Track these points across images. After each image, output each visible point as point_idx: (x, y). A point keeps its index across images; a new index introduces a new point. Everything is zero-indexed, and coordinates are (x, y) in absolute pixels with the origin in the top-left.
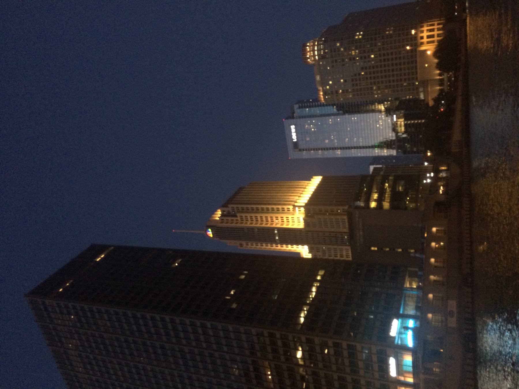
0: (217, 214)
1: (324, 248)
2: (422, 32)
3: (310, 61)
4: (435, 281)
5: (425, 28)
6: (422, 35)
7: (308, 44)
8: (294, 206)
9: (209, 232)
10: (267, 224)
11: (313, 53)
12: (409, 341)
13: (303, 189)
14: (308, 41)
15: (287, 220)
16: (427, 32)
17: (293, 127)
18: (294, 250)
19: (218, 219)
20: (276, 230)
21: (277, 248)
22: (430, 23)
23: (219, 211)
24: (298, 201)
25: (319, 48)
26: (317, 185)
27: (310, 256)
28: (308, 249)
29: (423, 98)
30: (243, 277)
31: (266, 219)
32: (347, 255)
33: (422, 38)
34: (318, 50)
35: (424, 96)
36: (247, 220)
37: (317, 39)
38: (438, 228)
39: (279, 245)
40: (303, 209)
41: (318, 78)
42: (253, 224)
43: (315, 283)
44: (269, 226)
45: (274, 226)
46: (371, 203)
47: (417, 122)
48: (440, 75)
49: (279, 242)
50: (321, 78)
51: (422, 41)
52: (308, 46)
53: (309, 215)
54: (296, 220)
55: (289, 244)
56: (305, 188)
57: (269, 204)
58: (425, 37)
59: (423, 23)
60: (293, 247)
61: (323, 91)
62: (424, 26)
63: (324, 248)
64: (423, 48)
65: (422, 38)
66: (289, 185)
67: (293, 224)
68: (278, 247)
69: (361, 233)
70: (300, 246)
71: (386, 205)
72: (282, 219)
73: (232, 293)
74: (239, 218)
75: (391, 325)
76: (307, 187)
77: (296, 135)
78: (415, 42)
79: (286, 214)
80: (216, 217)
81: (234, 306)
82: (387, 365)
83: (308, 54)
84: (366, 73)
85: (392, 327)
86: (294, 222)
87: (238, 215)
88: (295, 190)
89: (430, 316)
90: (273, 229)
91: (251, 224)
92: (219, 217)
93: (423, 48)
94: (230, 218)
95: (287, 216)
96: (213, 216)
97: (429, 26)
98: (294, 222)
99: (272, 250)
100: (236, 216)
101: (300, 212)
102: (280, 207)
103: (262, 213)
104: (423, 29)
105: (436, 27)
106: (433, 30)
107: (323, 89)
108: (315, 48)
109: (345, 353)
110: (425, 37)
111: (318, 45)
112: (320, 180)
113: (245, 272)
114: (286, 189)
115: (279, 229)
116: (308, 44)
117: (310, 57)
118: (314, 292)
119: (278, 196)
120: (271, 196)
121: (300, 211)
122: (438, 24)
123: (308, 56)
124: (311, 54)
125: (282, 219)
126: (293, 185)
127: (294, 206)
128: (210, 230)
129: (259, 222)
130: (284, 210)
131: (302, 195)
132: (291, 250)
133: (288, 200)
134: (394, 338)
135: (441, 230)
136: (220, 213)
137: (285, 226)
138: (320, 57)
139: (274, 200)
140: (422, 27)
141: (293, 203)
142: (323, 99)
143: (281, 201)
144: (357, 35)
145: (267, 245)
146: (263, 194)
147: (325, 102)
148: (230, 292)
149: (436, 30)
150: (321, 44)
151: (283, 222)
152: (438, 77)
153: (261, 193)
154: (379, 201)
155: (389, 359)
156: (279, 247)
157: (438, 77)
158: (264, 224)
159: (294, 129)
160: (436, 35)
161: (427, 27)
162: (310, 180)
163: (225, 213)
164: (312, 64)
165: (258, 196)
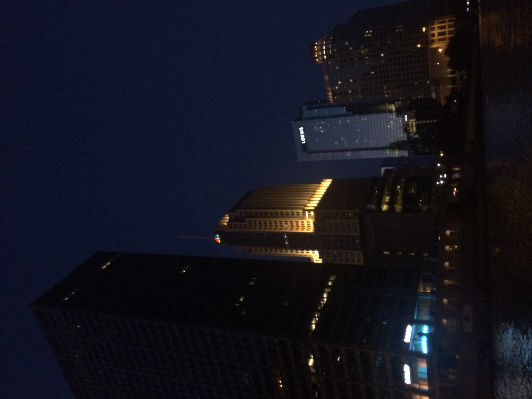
0: (225, 219)
1: (335, 253)
2: (433, 29)
4: (449, 285)
5: (436, 26)
6: (433, 32)
7: (316, 44)
8: (304, 211)
9: (217, 237)
11: (321, 53)
13: (312, 193)
16: (438, 30)
17: (301, 129)
19: (226, 224)
20: (285, 235)
21: (287, 253)
23: (227, 217)
24: (308, 205)
27: (320, 261)
33: (433, 35)
34: (326, 50)
40: (312, 213)
41: (327, 78)
44: (278, 230)
45: (283, 230)
48: (452, 73)
51: (433, 38)
52: (316, 45)
54: (306, 224)
55: (305, 250)
56: (315, 191)
58: (436, 35)
65: (433, 35)
70: (310, 252)
71: (398, 208)
72: (297, 223)
73: (241, 300)
74: (247, 223)
80: (224, 222)
84: (376, 73)
87: (246, 220)
89: (445, 321)
90: (283, 234)
91: (250, 228)
92: (227, 223)
93: (434, 46)
94: (238, 224)
95: (291, 220)
100: (244, 221)
102: (289, 211)
105: (447, 24)
106: (444, 27)
107: (332, 89)
112: (330, 183)
115: (289, 234)
116: (316, 44)
125: (291, 224)
128: (218, 236)
133: (298, 204)
134: (408, 344)
136: (228, 218)
137: (294, 231)
140: (433, 24)
141: (303, 207)
146: (271, 198)
149: (447, 27)
154: (391, 204)
157: (450, 76)
159: (303, 131)
160: (447, 33)
162: (320, 183)
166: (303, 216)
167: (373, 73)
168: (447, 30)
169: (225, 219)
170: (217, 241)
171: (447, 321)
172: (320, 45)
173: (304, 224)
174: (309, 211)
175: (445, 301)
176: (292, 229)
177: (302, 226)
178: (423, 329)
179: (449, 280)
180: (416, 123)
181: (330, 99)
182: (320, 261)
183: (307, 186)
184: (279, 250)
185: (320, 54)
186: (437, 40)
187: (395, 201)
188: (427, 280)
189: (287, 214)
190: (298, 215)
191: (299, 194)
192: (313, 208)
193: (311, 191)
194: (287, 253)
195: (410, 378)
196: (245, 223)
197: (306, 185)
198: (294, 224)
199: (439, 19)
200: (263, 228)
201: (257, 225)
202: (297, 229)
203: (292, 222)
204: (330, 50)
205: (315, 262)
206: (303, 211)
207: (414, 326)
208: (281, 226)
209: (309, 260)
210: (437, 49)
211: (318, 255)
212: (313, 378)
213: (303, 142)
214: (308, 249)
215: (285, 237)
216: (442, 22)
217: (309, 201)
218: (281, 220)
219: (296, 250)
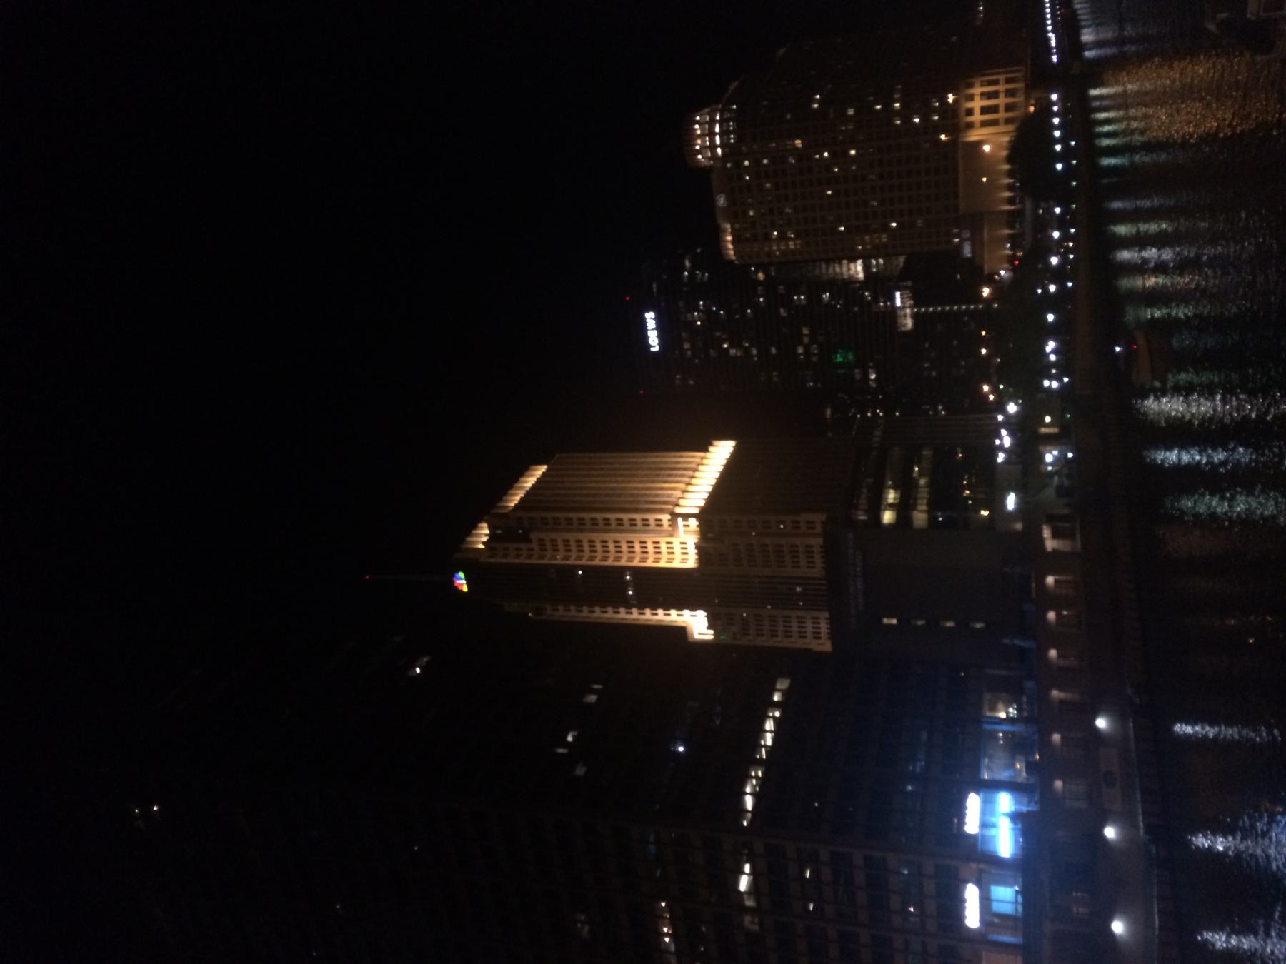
0: (480, 535)
1: (745, 615)
2: (971, 98)
3: (703, 160)
4: (1062, 702)
5: (977, 90)
6: (969, 105)
7: (698, 118)
8: (675, 516)
9: (460, 579)
10: (605, 559)
11: (710, 141)
12: (1005, 843)
13: (690, 473)
14: (698, 110)
15: (655, 548)
16: (981, 99)
17: (650, 318)
18: (671, 621)
19: (482, 546)
20: (628, 573)
21: (642, 617)
22: (990, 78)
23: (482, 528)
24: (682, 502)
25: (725, 128)
26: (724, 462)
27: (709, 635)
28: (706, 619)
29: (969, 255)
30: (592, 698)
31: (616, 547)
32: (800, 632)
33: (970, 112)
34: (721, 134)
35: (973, 251)
36: (554, 550)
37: (720, 106)
38: (1057, 577)
39: (635, 611)
40: (693, 523)
41: (721, 201)
42: (584, 559)
43: (770, 709)
44: (610, 562)
45: (623, 563)
46: (882, 512)
47: (941, 310)
48: (1010, 201)
49: (635, 602)
50: (731, 201)
51: (970, 119)
52: (698, 122)
53: (710, 535)
54: (677, 548)
55: (660, 608)
56: (696, 470)
57: (636, 510)
58: (977, 111)
59: (971, 77)
60: (682, 615)
61: (732, 233)
62: (976, 85)
63: (745, 615)
64: (973, 136)
65: (970, 112)
66: (654, 463)
67: (669, 559)
68: (606, 612)
69: (860, 585)
70: (686, 612)
71: (920, 517)
72: (631, 545)
73: (570, 739)
74: (534, 545)
75: (965, 808)
76: (701, 468)
77: (657, 337)
78: (954, 120)
79: (655, 533)
80: (477, 542)
81: (580, 771)
82: (959, 902)
83: (699, 141)
84: (836, 193)
85: (967, 812)
86: (673, 553)
87: (533, 536)
88: (670, 476)
89: (1058, 784)
90: (623, 570)
91: (543, 557)
92: (484, 543)
93: (973, 136)
95: (657, 540)
96: (469, 539)
97: (985, 83)
98: (673, 553)
99: (592, 620)
100: (530, 541)
101: (687, 529)
102: (638, 517)
103: (593, 531)
104: (971, 91)
105: (1001, 88)
106: (994, 95)
107: (732, 228)
108: (714, 128)
109: (860, 878)
110: (977, 111)
111: (721, 122)
112: (731, 450)
113: (596, 686)
114: (649, 472)
115: (637, 572)
116: (698, 118)
117: (703, 151)
118: (768, 732)
119: (631, 489)
120: (612, 489)
121: (688, 526)
122: (1008, 81)
123: (698, 147)
124: (706, 141)
125: (642, 547)
126: (666, 463)
127: (675, 516)
128: (461, 574)
129: (587, 553)
130: (648, 525)
131: (690, 488)
132: (638, 620)
133: (657, 499)
134: (974, 837)
135: (1065, 581)
136: (487, 532)
137: (650, 563)
138: (727, 150)
139: (622, 499)
140: (971, 86)
141: (670, 507)
142: (732, 253)
143: (639, 502)
144: (817, 99)
145: (616, 610)
146: (593, 485)
147: (737, 260)
148: (566, 736)
149: (1002, 95)
150: (728, 120)
151: (660, 553)
152: (1007, 207)
153: (610, 482)
154: (903, 508)
155: (965, 888)
156: (635, 615)
157: (1007, 207)
158: (612, 558)
159: (654, 322)
160: (1002, 108)
161: (982, 86)
162: (706, 450)
163: (499, 532)
164: (705, 166)
165: (581, 488)
166: (670, 529)
167: (829, 192)
168: (1002, 101)
169: (480, 535)
170: (460, 588)
171: (1064, 783)
172: (707, 122)
173: (659, 548)
174: (686, 517)
175: (1056, 737)
176: (644, 560)
177: (669, 553)
178: (997, 800)
179: (1060, 689)
180: (912, 311)
181: (729, 249)
182: (709, 635)
183: (675, 457)
184: (572, 608)
185: (708, 143)
186: (977, 124)
187: (911, 502)
188: (1012, 692)
189: (633, 522)
190: (658, 525)
191: (658, 475)
192: (696, 511)
193: (685, 469)
194: (642, 617)
195: (746, 886)
196: (529, 546)
197: (673, 454)
198: (650, 547)
199: (983, 75)
200: (587, 557)
201: (558, 550)
202: (629, 558)
203: (645, 542)
204: (732, 136)
205: (697, 637)
206: (672, 517)
207: (981, 794)
208: (617, 552)
209: (682, 631)
210: (979, 144)
211: (706, 620)
212: (747, 919)
213: (654, 347)
214: (680, 607)
215: (628, 578)
216: (990, 83)
217: (683, 494)
218: (605, 539)
219: (614, 607)
